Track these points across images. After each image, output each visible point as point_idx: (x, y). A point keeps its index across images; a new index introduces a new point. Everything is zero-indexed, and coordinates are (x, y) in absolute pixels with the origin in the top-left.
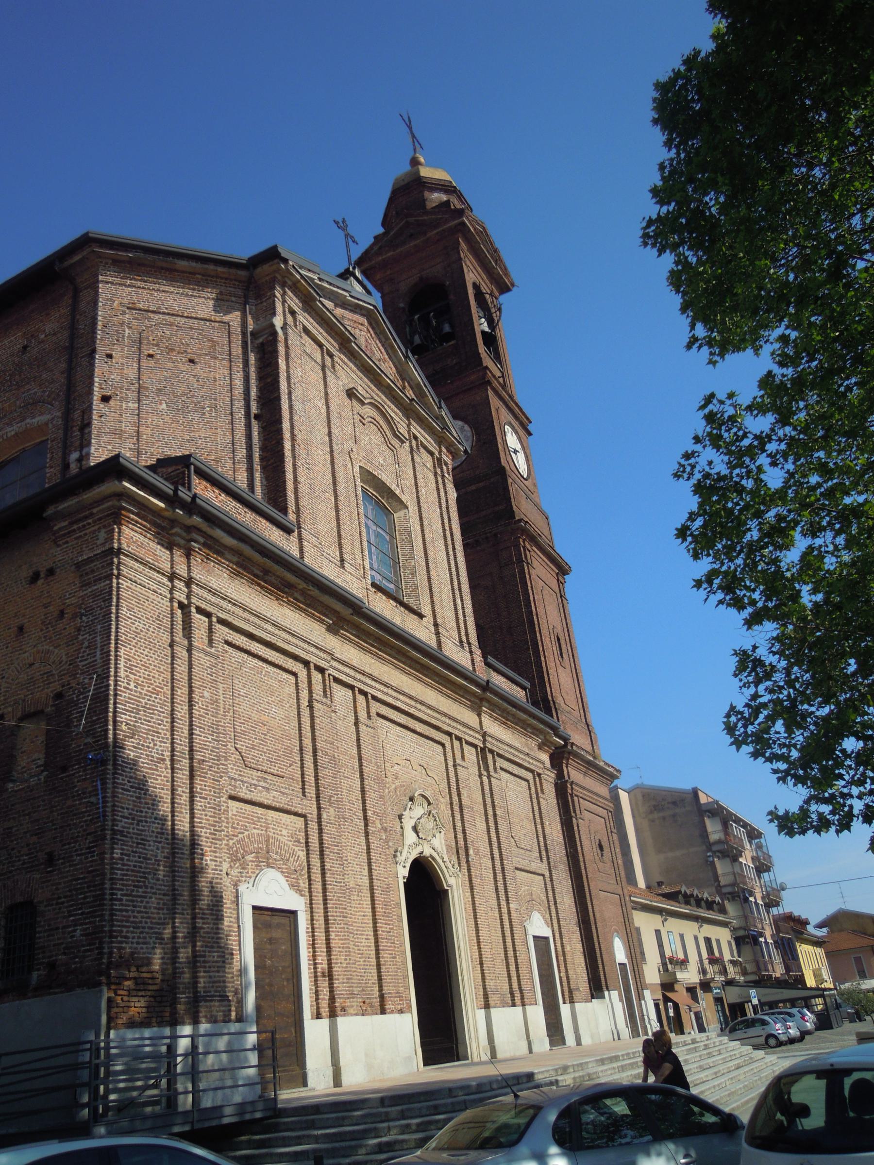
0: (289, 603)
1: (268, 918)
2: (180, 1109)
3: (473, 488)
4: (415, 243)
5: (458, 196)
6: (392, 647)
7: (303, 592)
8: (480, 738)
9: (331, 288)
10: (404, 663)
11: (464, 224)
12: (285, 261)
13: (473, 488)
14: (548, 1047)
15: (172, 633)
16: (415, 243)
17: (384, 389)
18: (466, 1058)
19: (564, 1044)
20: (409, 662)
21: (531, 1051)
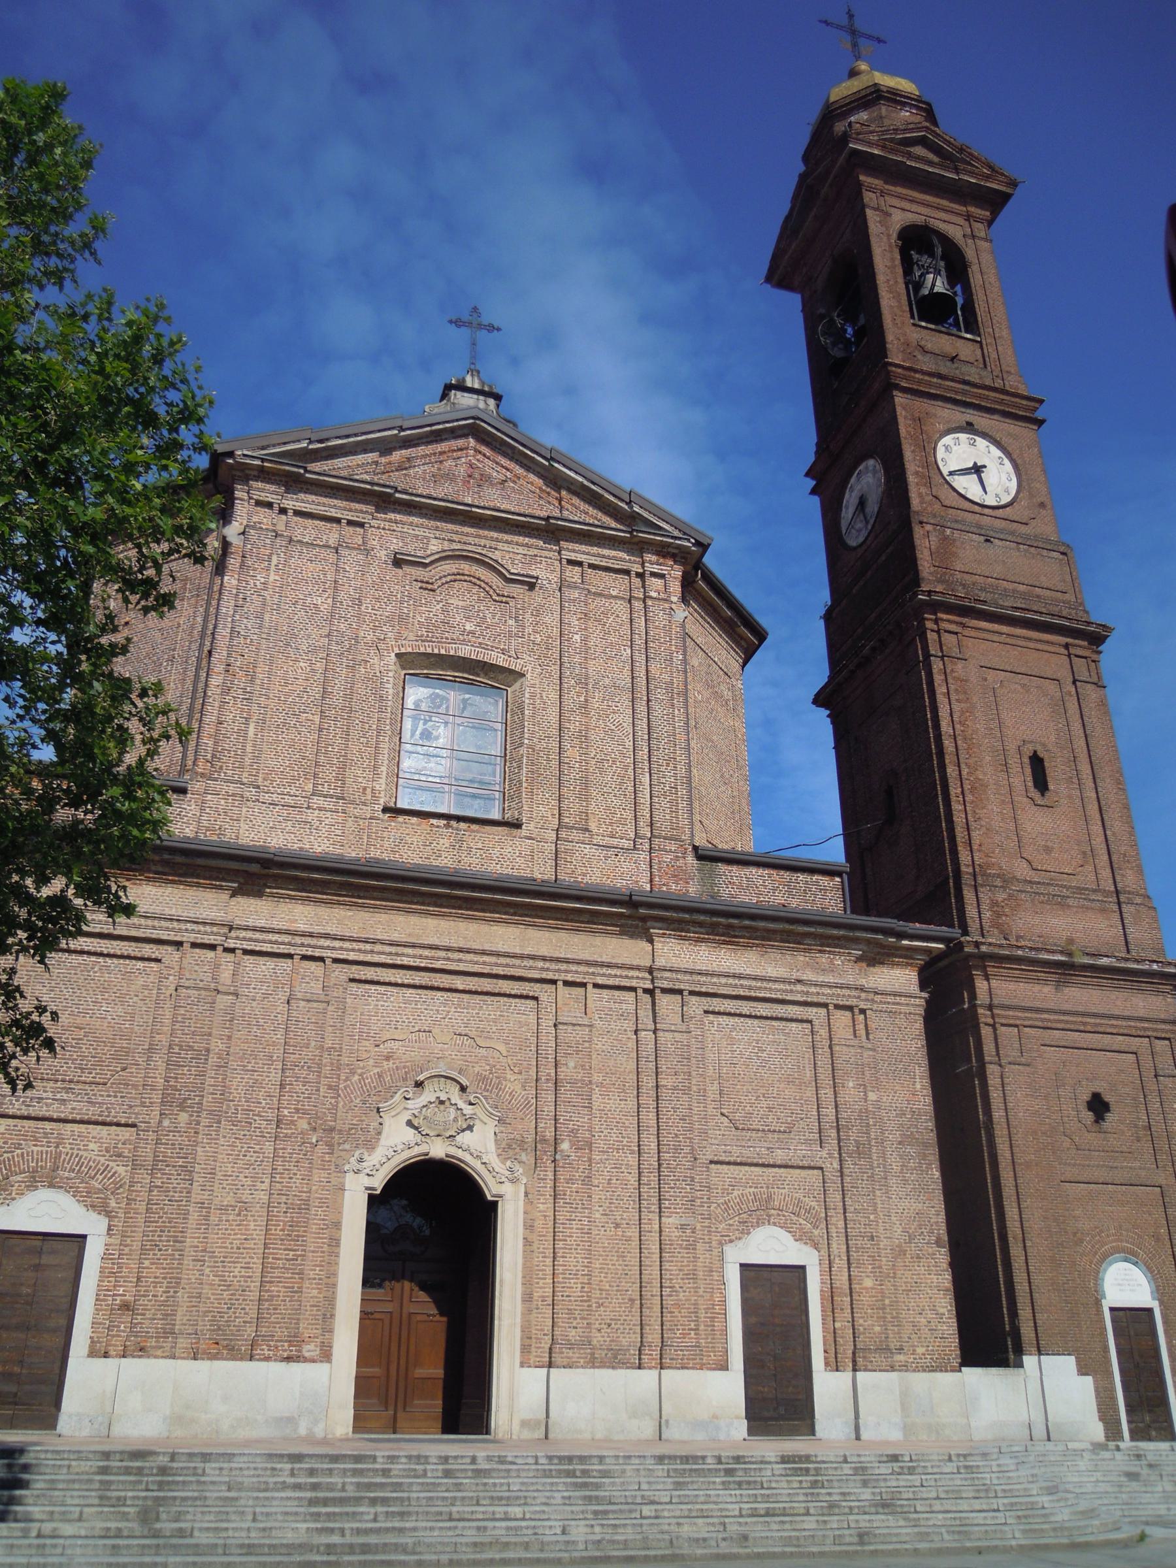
0: (148, 879)
1: (38, 1243)
2: (901, 1438)
3: (883, 558)
4: (812, 214)
5: (888, 99)
6: (375, 888)
7: (166, 863)
8: (647, 975)
9: (351, 440)
10: (423, 904)
11: (856, 152)
12: (231, 454)
13: (883, 558)
14: (743, 1431)
15: (556, 860)
16: (812, 214)
17: (493, 524)
18: (488, 1432)
19: (813, 1433)
20: (427, 900)
21: (546, 1437)
